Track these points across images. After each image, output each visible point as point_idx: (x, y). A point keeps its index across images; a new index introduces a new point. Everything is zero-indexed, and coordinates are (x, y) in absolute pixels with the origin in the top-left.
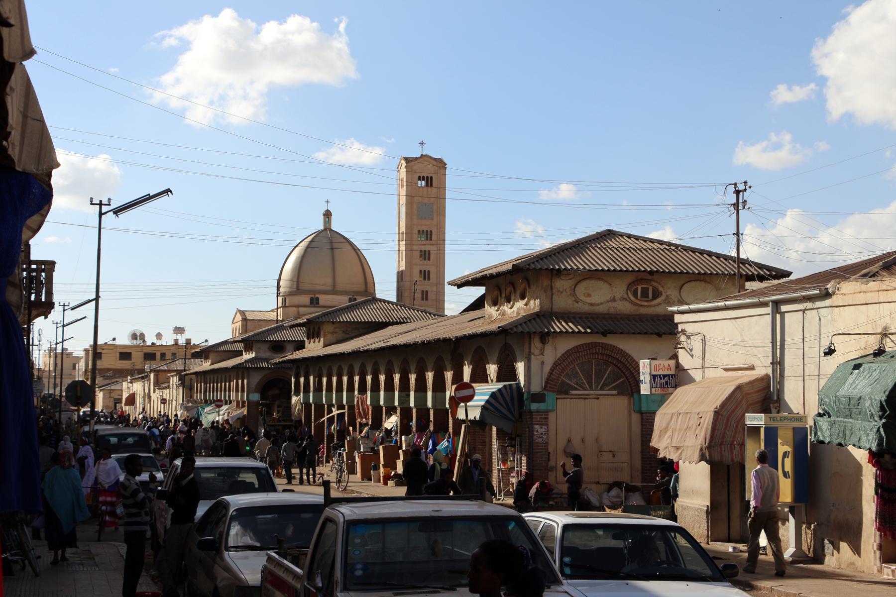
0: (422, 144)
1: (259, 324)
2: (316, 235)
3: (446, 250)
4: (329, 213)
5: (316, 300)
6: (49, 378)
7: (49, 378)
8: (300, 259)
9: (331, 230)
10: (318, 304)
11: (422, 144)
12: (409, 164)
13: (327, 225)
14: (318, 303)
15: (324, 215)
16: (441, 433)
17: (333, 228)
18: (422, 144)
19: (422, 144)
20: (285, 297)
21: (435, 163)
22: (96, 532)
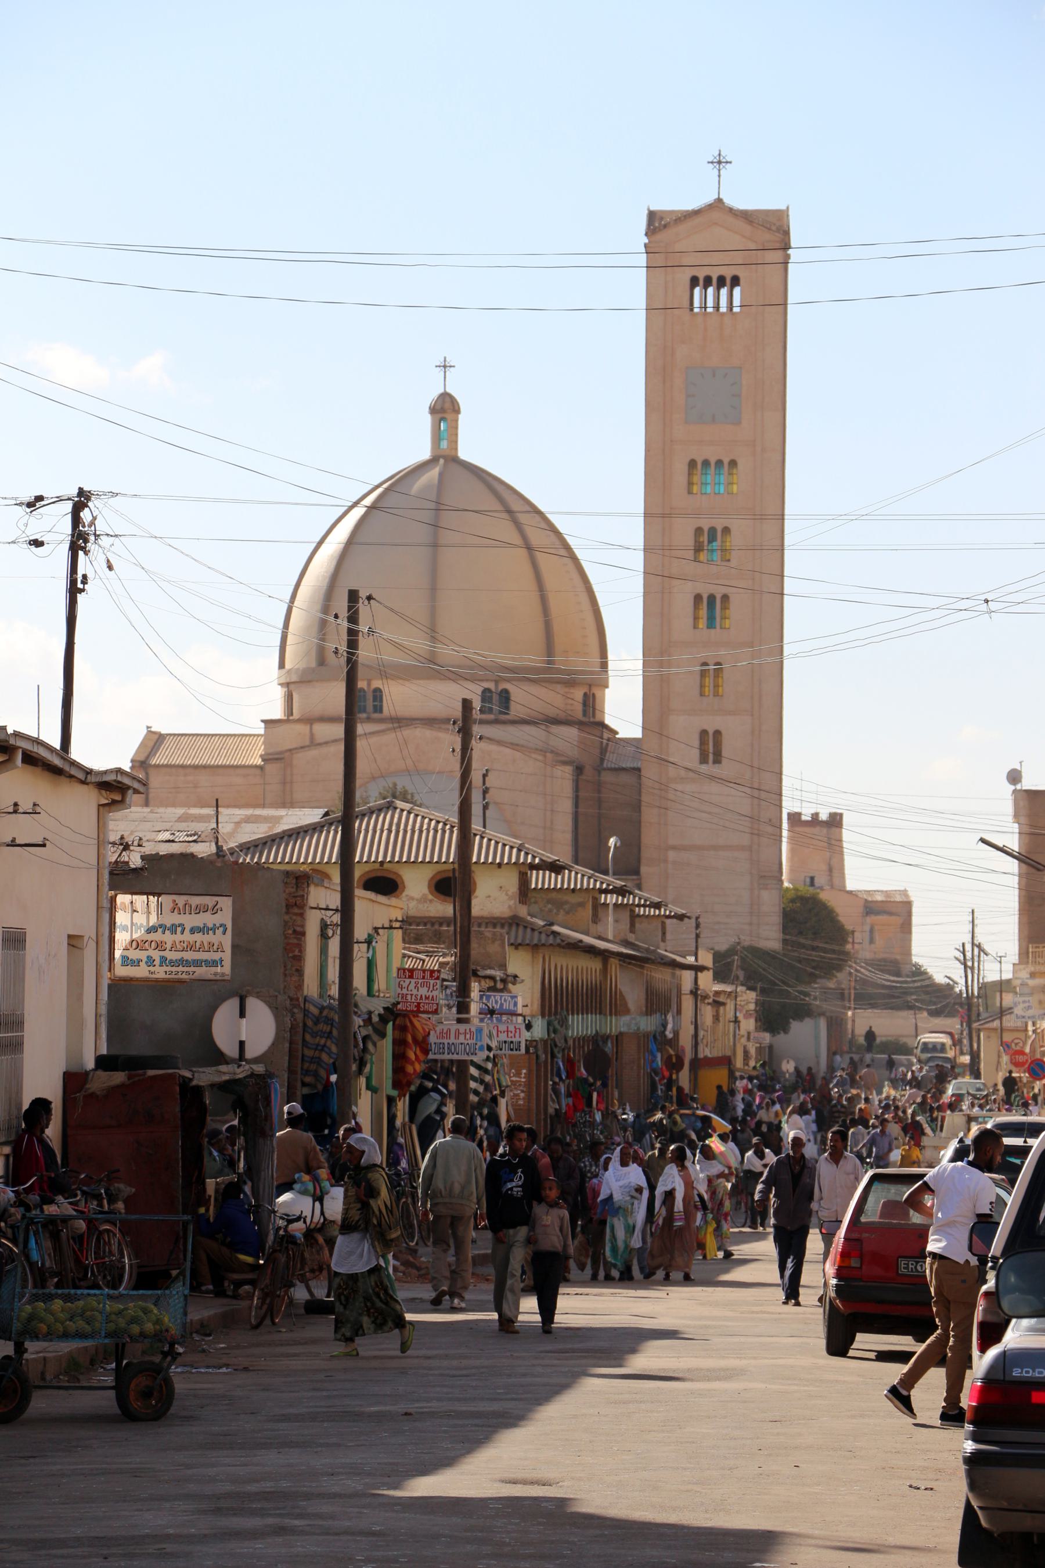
0: (719, 162)
1: (190, 778)
2: (387, 490)
3: (642, 553)
4: (448, 405)
5: (375, 699)
6: (217, 807)
7: (217, 807)
8: (334, 563)
9: (455, 460)
10: (381, 711)
11: (719, 162)
12: (658, 237)
13: (444, 444)
14: (378, 709)
15: (433, 410)
16: (790, 1074)
17: (464, 454)
18: (719, 162)
19: (719, 162)
20: (292, 687)
21: (741, 224)
22: (189, 1418)
